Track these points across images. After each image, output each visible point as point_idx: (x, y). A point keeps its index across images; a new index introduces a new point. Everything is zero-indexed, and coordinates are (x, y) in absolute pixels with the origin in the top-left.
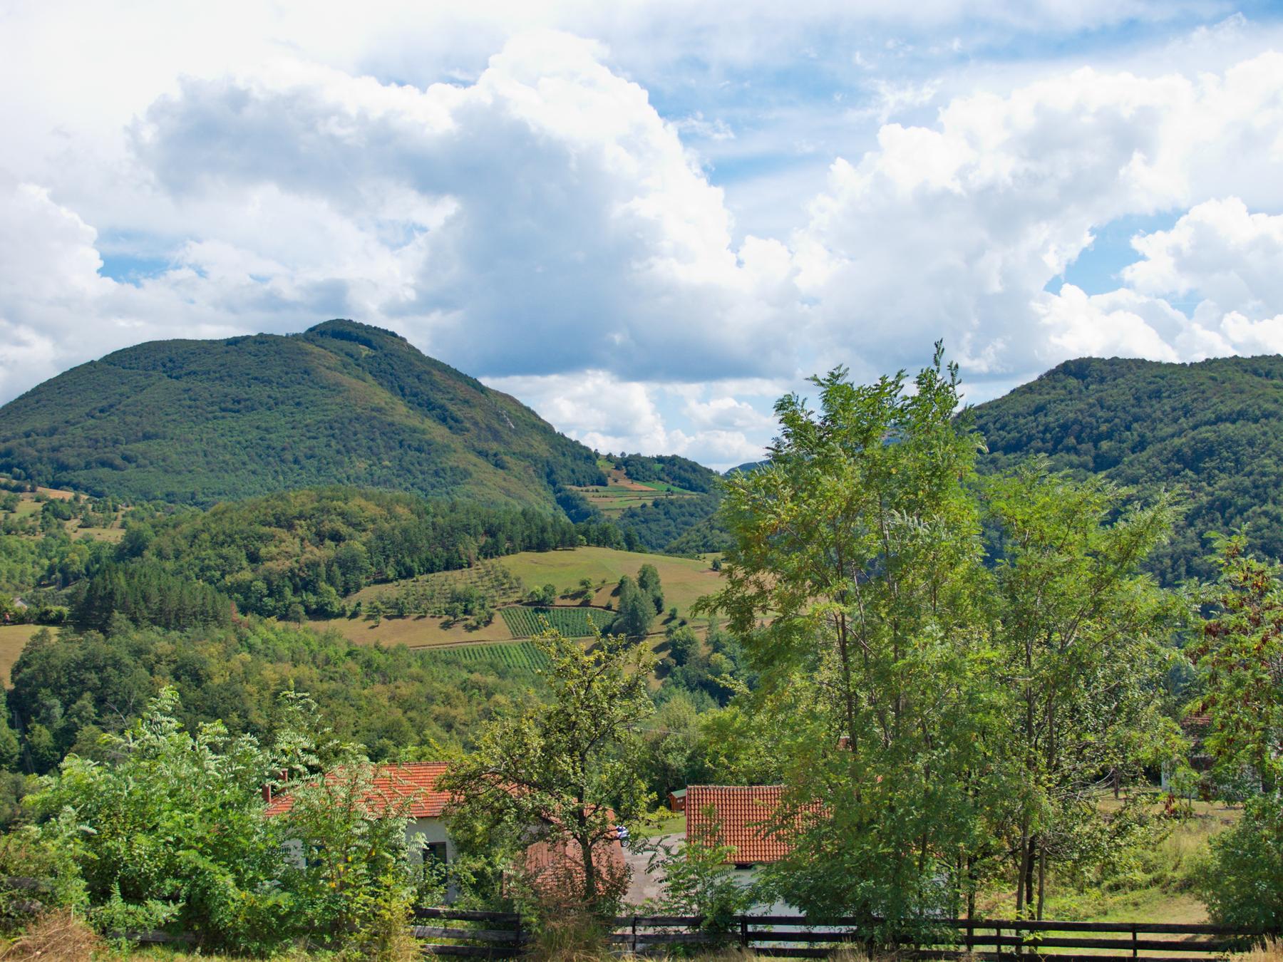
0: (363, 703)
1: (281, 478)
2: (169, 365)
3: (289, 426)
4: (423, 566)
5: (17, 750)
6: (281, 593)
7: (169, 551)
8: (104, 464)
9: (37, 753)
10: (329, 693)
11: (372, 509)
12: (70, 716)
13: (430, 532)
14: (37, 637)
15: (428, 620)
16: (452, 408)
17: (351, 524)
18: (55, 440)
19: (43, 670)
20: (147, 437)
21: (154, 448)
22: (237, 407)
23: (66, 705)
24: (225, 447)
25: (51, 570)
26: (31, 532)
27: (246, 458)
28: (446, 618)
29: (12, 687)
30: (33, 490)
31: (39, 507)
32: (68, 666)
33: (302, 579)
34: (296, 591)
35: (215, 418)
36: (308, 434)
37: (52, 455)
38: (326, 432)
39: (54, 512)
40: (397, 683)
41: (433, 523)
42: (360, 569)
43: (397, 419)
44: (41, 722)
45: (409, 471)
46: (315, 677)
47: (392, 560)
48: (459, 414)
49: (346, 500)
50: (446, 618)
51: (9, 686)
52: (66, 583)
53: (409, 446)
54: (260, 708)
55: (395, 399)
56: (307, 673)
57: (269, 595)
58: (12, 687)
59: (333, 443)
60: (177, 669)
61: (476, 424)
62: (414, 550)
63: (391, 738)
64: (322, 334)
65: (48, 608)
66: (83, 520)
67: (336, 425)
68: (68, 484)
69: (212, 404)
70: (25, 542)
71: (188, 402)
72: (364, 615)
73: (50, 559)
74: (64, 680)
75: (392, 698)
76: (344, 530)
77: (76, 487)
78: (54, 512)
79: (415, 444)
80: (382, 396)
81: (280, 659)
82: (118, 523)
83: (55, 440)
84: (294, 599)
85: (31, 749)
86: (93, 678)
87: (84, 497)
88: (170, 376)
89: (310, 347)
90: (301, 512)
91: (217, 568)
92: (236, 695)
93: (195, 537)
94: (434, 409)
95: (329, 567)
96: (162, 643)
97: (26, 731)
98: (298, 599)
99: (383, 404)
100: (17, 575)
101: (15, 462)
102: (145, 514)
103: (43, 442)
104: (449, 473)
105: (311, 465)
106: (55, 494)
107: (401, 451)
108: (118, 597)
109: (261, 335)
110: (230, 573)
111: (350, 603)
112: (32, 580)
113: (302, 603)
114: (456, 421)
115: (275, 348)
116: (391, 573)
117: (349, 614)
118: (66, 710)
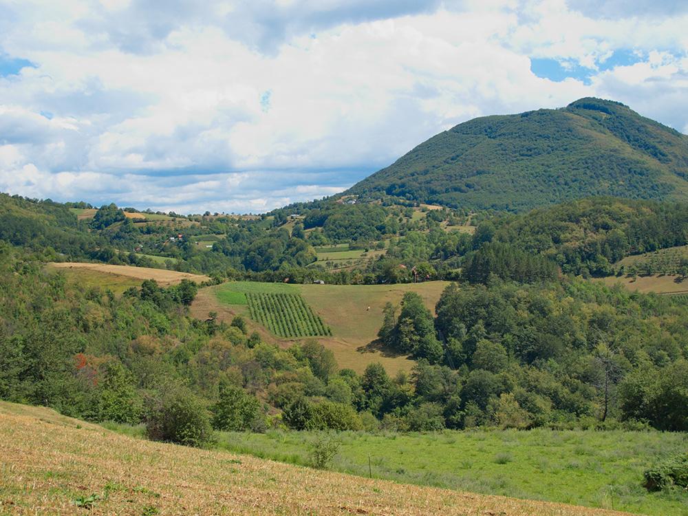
0: (645, 328)
1: (558, 194)
2: (489, 130)
3: (561, 163)
4: (661, 244)
5: (442, 352)
6: (574, 261)
7: (506, 237)
8: (456, 189)
9: (454, 355)
10: (623, 321)
11: (627, 210)
12: (471, 334)
13: (665, 223)
14: (448, 288)
15: (666, 277)
16: (660, 147)
17: (614, 219)
18: (428, 177)
19: (454, 307)
20: (479, 173)
21: (483, 179)
22: (530, 153)
23: (469, 327)
24: (524, 177)
25: (437, 250)
26: (422, 228)
27: (537, 183)
28: (677, 276)
29: (436, 316)
30: (418, 206)
31: (424, 214)
32: (468, 304)
33: (586, 253)
34: (583, 260)
35: (517, 160)
36: (573, 167)
37: (427, 185)
38: (583, 166)
39: (433, 218)
40: (664, 316)
41: (666, 218)
42: (622, 247)
43: (626, 156)
44: (455, 336)
45: (635, 187)
46: (613, 311)
47: (641, 240)
48: (665, 151)
49: (610, 204)
50: (677, 276)
51: (435, 316)
52: (446, 258)
53: (635, 172)
54: (582, 330)
55: (624, 144)
56: (609, 309)
57: (567, 263)
58: (436, 316)
59: (588, 172)
60: (530, 306)
61: (676, 156)
62: (654, 234)
63: (665, 350)
64: (578, 107)
65: (450, 270)
66: (450, 221)
67: (589, 161)
68: (436, 202)
69: (515, 152)
70: (420, 235)
71: (502, 152)
72: (626, 274)
73: (436, 244)
74: (466, 313)
75: (662, 325)
76: (610, 222)
77: (441, 204)
78: (433, 218)
79: (638, 170)
80: (616, 142)
81: (590, 301)
82: (469, 222)
83: (428, 177)
84: (582, 265)
85: (450, 352)
86: (483, 311)
87: (448, 209)
88: (490, 137)
89: (570, 115)
90: (584, 212)
91: (535, 247)
92: (568, 322)
93: (521, 229)
94: (648, 148)
95: (603, 245)
96: (520, 291)
97: (447, 342)
98: (585, 265)
99: (617, 147)
100: (419, 253)
101: (407, 190)
102: (484, 218)
103: (422, 178)
104: (661, 188)
105: (576, 185)
106: (431, 207)
107: (630, 175)
108: (492, 263)
109: (541, 110)
110: (543, 250)
111: (617, 267)
112: (427, 256)
113: (588, 267)
114: (663, 155)
115: (550, 117)
116: (641, 249)
117: (616, 273)
118: (468, 330)
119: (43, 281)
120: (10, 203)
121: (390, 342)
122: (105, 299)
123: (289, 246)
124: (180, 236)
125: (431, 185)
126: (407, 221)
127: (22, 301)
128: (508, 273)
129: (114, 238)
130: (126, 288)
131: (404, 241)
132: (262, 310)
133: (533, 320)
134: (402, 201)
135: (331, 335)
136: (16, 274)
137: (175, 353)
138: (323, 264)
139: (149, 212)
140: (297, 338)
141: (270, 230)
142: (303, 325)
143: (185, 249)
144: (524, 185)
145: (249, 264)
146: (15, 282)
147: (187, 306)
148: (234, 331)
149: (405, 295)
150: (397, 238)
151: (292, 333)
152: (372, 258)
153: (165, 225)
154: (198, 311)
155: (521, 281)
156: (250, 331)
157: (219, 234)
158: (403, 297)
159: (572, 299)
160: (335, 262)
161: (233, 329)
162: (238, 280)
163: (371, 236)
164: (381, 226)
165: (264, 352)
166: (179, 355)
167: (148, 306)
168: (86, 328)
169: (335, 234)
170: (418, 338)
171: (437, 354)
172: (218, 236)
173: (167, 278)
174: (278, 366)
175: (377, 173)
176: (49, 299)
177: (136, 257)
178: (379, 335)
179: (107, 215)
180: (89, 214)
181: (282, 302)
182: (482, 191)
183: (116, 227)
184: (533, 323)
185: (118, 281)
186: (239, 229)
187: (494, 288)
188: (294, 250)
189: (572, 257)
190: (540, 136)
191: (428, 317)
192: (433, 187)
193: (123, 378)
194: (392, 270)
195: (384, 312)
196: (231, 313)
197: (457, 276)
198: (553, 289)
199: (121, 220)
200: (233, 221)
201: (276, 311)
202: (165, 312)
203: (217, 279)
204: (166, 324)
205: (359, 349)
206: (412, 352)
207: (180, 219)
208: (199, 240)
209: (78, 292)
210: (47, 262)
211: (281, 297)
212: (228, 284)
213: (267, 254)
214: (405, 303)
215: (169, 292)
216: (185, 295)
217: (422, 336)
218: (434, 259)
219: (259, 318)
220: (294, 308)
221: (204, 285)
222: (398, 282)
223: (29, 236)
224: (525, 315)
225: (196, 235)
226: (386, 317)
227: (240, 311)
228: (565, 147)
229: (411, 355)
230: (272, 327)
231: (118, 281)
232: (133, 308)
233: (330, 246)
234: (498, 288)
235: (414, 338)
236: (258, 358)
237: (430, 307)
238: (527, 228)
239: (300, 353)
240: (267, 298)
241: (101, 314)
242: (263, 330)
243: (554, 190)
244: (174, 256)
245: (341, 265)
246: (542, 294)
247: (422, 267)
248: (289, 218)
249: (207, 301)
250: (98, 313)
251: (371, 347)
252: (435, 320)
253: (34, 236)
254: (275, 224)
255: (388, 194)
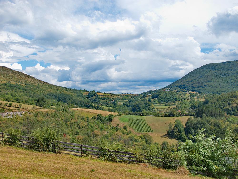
1: (234, 88)
2: (212, 68)
8: (201, 87)
12: (195, 133)
14: (189, 118)
18: (192, 83)
20: (208, 81)
21: (210, 84)
22: (225, 75)
23: (195, 131)
24: (223, 83)
26: (188, 99)
27: (227, 85)
29: (185, 127)
30: (188, 92)
31: (189, 95)
39: (192, 96)
51: (185, 127)
52: (194, 109)
60: (215, 125)
66: (197, 97)
68: (194, 91)
69: (221, 75)
70: (187, 101)
74: (194, 126)
77: (196, 91)
81: (235, 123)
82: (204, 97)
83: (192, 83)
96: (212, 120)
97: (188, 135)
100: (186, 107)
102: (209, 96)
103: (190, 83)
106: (192, 92)
108: (204, 111)
110: (225, 107)
119: (68, 113)
120: (63, 90)
121: (171, 135)
122: (86, 119)
123: (146, 104)
124: (113, 100)
125: (193, 85)
126: (184, 97)
127: (62, 119)
128: (209, 114)
129: (94, 101)
130: (92, 116)
131: (182, 103)
132: (133, 124)
133: (215, 129)
134: (183, 90)
135: (153, 132)
136: (61, 111)
137: (105, 136)
138: (156, 110)
139: (104, 93)
140: (142, 133)
141: (141, 99)
142: (145, 129)
143: (114, 105)
144: (223, 86)
145: (134, 110)
146: (60, 113)
147: (111, 122)
148: (123, 130)
149: (176, 120)
150: (180, 102)
151: (141, 131)
152: (172, 108)
153: (109, 97)
154: (113, 124)
155: (213, 117)
156: (128, 130)
157: (125, 100)
158: (175, 121)
159: (228, 123)
160: (160, 109)
161: (123, 129)
162: (127, 114)
163: (172, 101)
164: (176, 98)
165: (131, 136)
166: (106, 137)
167: (99, 122)
168: (79, 128)
169: (161, 100)
170: (179, 133)
171: (185, 139)
172: (125, 101)
173: (105, 113)
174: (136, 141)
175: (176, 81)
176: (70, 119)
177: (99, 107)
178: (167, 133)
179: (92, 94)
180: (85, 94)
181: (139, 121)
182: (209, 87)
183: (94, 97)
184: (215, 130)
185: (91, 114)
186: (131, 99)
187: (204, 118)
188: (147, 106)
189: (234, 109)
190: (229, 70)
191: (183, 127)
192: (194, 86)
193: (77, 141)
194: (173, 112)
195: (169, 125)
196: (123, 124)
197: (193, 114)
198: (223, 119)
199: (96, 95)
200: (130, 96)
201: (137, 124)
202: (103, 124)
203: (120, 114)
204: (103, 127)
205: (161, 137)
206: (177, 138)
207: (114, 95)
208: (119, 102)
209: (78, 117)
210: (71, 108)
211: (139, 120)
212: (123, 116)
213: (139, 107)
214: (176, 123)
215: (105, 118)
216: (110, 119)
217: (180, 133)
218: (191, 109)
219: (132, 126)
220: (142, 123)
221: (116, 116)
222: (175, 116)
223: (68, 100)
224: (213, 127)
225: (118, 100)
226: (170, 127)
227: (126, 124)
228: (237, 73)
229: (177, 139)
230: (135, 129)
231: (91, 114)
232: (94, 122)
233: (159, 104)
234: (205, 119)
235: (178, 133)
236: (130, 138)
237: (183, 124)
238: (220, 100)
239: (143, 137)
240: (134, 120)
241: (84, 124)
242: (132, 130)
243: (233, 87)
244: (111, 107)
245: (162, 110)
246: (219, 121)
247: (182, 112)
248: (147, 95)
249: (116, 121)
250: (83, 123)
251: (165, 136)
252: (185, 128)
253: (70, 100)
254: (143, 97)
255: (179, 88)
